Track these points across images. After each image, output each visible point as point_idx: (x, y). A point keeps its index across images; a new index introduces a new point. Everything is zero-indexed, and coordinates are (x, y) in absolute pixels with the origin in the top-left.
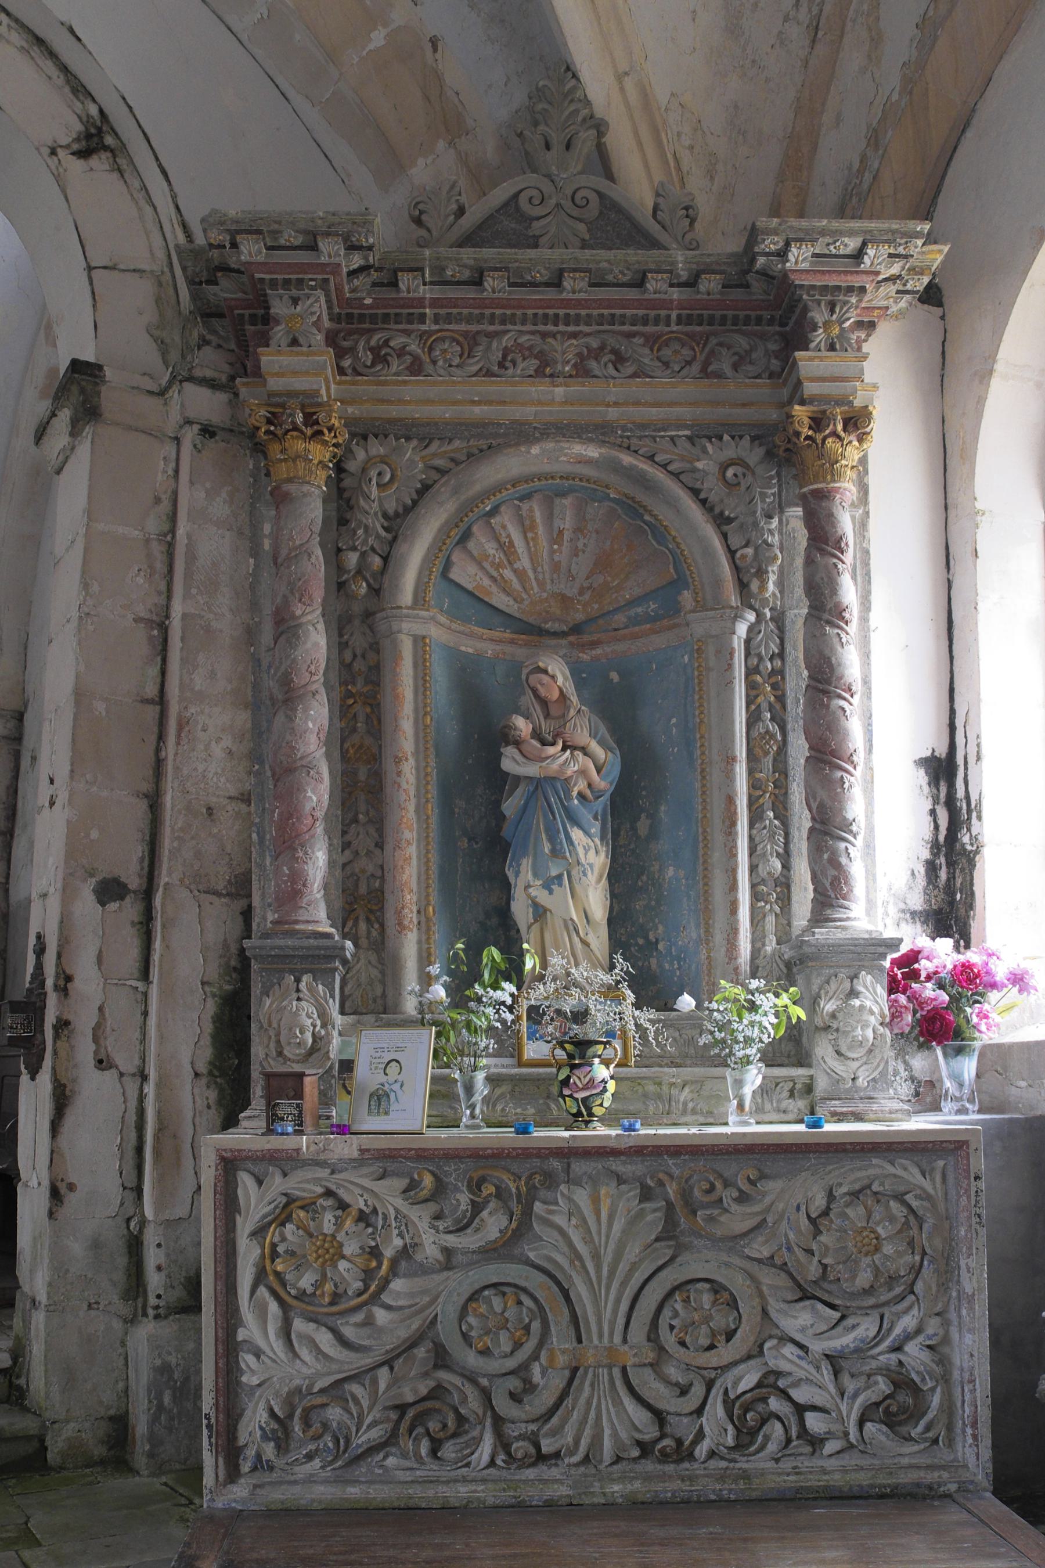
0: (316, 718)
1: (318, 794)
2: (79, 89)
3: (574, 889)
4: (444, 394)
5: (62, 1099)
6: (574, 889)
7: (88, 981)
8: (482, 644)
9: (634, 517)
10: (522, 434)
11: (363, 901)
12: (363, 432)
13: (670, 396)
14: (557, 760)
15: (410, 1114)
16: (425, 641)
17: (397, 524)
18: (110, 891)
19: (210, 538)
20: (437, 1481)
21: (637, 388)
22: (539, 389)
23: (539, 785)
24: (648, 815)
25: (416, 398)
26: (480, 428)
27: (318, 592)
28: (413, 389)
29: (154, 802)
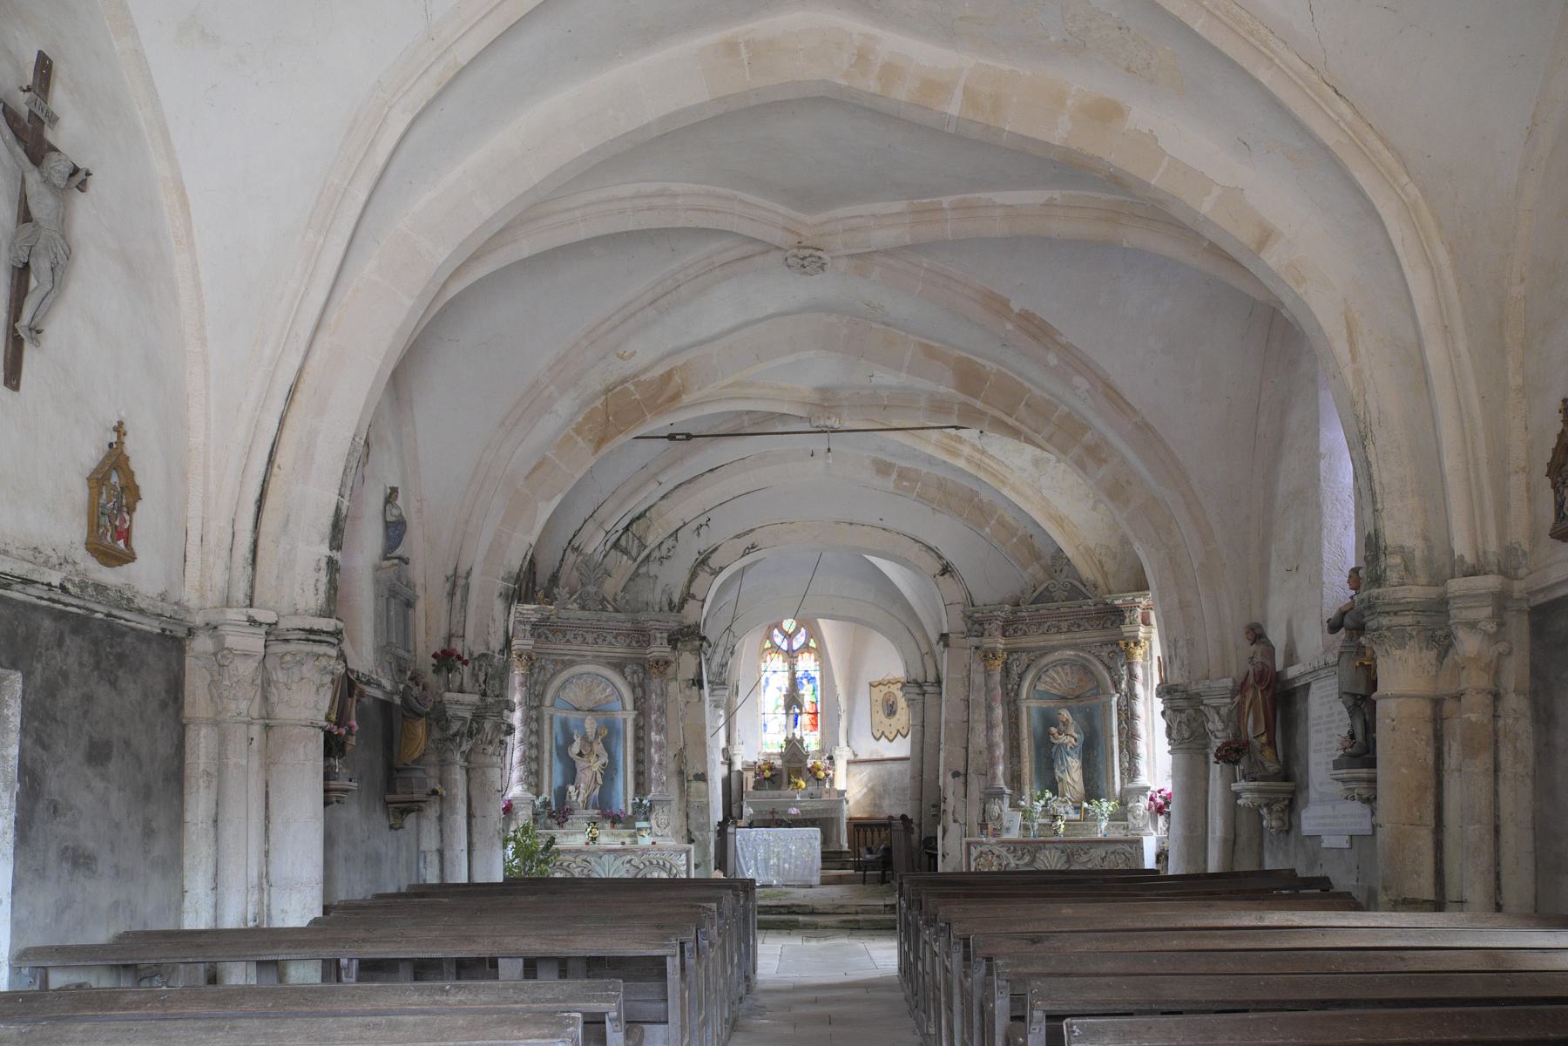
0: (999, 731)
1: (1000, 751)
2: (940, 557)
3: (1072, 773)
4: (1033, 641)
5: (945, 832)
6: (1072, 773)
7: (951, 800)
8: (1045, 704)
9: (1085, 670)
10: (1054, 649)
11: (1015, 779)
12: (1010, 652)
13: (1094, 636)
14: (1063, 739)
15: (1015, 834)
16: (1030, 709)
17: (1021, 677)
18: (956, 774)
19: (978, 678)
20: (59, 602)
21: (1084, 634)
22: (1057, 637)
23: (1060, 745)
24: (1092, 752)
25: (1024, 642)
26: (1044, 647)
27: (999, 698)
28: (1024, 639)
29: (967, 749)
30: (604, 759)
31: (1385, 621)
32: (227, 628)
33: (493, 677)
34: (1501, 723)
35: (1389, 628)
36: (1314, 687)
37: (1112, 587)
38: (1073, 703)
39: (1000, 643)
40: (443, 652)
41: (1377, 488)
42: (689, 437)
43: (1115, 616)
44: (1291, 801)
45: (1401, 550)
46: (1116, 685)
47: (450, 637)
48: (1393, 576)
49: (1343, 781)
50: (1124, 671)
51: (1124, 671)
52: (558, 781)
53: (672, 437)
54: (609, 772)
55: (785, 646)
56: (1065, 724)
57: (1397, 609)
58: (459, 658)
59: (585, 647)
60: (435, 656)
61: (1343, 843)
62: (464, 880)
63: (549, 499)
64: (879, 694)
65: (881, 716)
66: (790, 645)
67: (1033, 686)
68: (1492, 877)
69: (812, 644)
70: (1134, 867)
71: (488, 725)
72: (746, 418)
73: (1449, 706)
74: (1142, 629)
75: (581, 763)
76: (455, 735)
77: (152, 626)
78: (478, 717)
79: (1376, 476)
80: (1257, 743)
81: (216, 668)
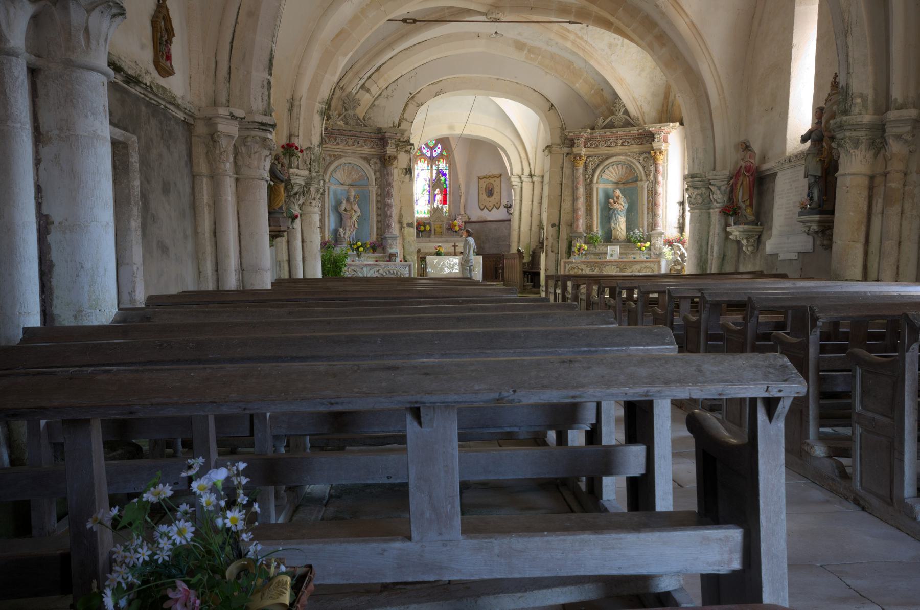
9: (630, 168)
13: (636, 148)
14: (616, 206)
17: (594, 171)
18: (553, 225)
19: (567, 171)
21: (631, 147)
28: (596, 149)
30: (359, 213)
31: (848, 134)
32: (219, 120)
33: (315, 161)
34: (907, 188)
35: (850, 138)
36: (779, 175)
37: (646, 121)
38: (621, 186)
39: (583, 151)
40: (288, 145)
41: (851, 60)
42: (415, 21)
43: (650, 137)
44: (760, 236)
45: (861, 95)
46: (647, 175)
47: (290, 136)
48: (856, 110)
49: (803, 222)
50: (652, 168)
51: (652, 168)
52: (333, 226)
53: (404, 21)
54: (362, 220)
55: (429, 154)
56: (618, 198)
57: (856, 127)
58: (297, 148)
59: (347, 147)
60: (283, 147)
61: (793, 256)
62: (302, 277)
63: (346, 55)
64: (484, 184)
65: (484, 196)
66: (432, 153)
67: (600, 176)
68: (895, 268)
69: (444, 153)
70: (656, 273)
71: (313, 189)
72: (447, 11)
73: (878, 181)
74: (664, 145)
75: (346, 215)
76: (296, 194)
77: (180, 115)
78: (308, 184)
79: (851, 54)
80: (743, 206)
81: (211, 143)
